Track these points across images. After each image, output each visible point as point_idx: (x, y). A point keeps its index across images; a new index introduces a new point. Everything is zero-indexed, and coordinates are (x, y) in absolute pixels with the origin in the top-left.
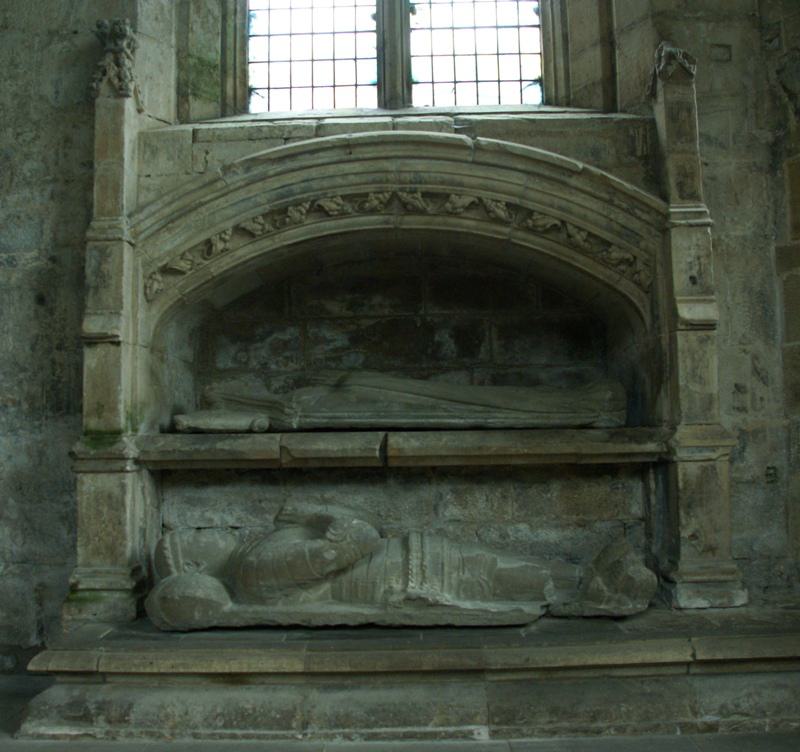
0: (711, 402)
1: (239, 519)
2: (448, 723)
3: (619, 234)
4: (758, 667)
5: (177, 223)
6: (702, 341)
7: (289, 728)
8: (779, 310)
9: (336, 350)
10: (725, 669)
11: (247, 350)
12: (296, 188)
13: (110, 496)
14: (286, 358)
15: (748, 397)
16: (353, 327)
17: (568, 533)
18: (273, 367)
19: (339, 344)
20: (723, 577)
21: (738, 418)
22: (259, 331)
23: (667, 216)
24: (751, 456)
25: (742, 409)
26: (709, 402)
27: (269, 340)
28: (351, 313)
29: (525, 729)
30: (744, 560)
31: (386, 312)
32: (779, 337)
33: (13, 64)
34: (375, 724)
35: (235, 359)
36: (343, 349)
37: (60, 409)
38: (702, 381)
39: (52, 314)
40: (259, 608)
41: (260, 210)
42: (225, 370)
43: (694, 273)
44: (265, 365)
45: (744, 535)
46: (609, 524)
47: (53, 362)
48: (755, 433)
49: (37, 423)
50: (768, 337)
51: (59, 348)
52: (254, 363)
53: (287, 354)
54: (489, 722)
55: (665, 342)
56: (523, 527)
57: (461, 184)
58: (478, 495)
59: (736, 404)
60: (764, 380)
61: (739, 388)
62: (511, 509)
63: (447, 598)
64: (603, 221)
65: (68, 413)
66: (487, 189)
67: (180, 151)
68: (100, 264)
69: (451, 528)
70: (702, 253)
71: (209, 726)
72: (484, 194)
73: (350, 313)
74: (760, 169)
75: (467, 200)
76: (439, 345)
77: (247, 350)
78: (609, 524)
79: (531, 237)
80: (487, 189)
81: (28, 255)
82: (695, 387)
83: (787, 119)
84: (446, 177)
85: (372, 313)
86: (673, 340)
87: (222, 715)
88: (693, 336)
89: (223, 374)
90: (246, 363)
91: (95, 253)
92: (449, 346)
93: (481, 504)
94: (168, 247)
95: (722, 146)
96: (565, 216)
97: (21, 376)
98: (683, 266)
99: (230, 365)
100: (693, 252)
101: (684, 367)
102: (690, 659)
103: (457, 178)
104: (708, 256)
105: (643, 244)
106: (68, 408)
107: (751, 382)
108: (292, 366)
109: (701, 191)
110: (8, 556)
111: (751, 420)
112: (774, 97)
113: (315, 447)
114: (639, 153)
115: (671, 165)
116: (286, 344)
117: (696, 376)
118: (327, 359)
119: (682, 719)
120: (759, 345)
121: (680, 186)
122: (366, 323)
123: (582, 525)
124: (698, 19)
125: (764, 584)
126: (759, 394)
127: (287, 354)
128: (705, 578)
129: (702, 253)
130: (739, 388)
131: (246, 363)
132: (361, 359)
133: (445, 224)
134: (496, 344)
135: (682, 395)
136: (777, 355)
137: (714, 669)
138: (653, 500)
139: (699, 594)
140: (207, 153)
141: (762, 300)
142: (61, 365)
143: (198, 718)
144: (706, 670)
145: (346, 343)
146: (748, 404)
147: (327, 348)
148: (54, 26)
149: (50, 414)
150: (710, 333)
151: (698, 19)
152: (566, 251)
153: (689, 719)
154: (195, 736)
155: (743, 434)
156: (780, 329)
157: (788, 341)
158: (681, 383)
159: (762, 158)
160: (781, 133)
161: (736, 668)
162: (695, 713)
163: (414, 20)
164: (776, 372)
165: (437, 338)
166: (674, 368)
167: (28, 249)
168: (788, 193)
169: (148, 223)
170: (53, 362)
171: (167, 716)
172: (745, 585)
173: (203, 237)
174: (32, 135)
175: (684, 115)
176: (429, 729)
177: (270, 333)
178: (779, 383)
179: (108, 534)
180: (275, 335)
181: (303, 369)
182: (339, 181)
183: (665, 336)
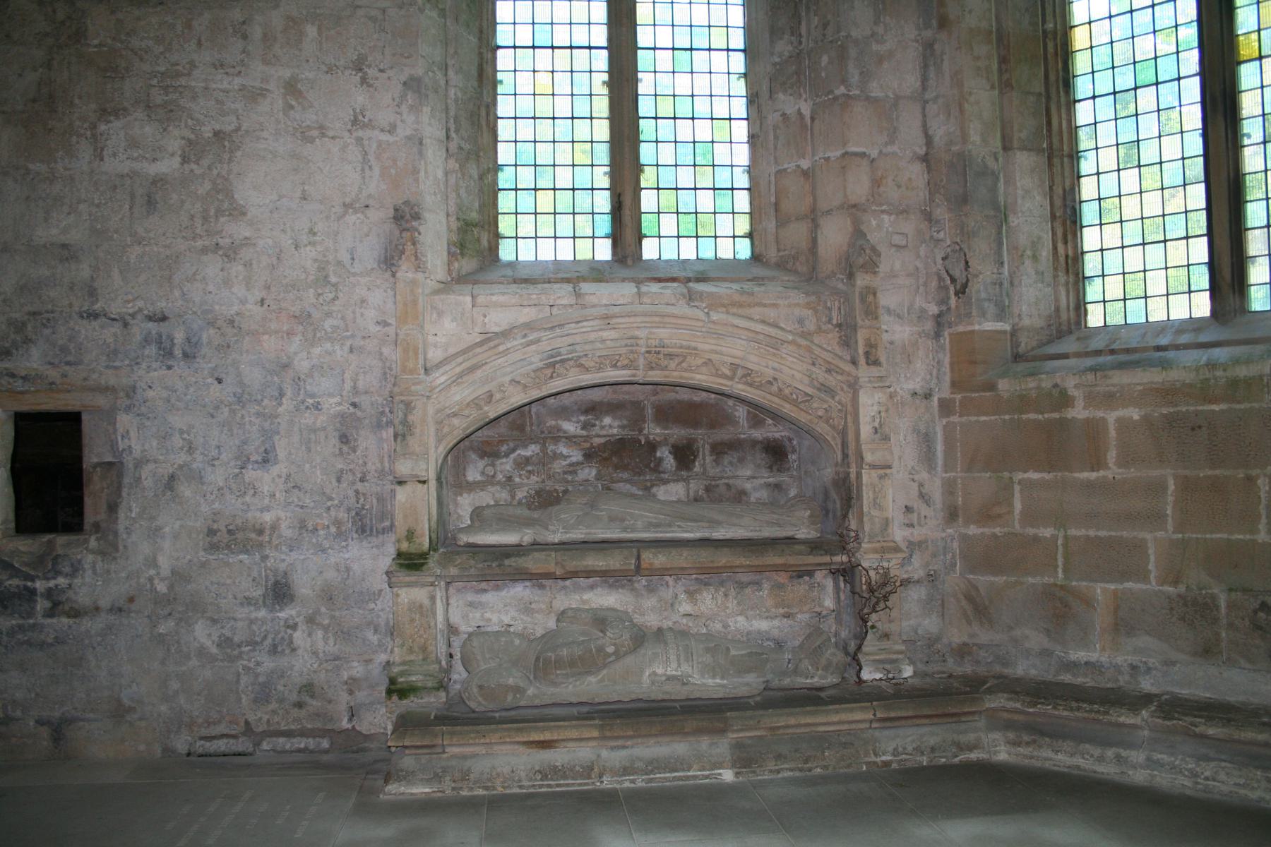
0: (887, 525)
1: (513, 618)
2: (703, 769)
3: (819, 389)
4: (918, 721)
5: (465, 378)
6: (881, 477)
7: (589, 777)
8: (940, 448)
9: (571, 465)
10: (897, 723)
11: (493, 465)
12: (563, 351)
13: (421, 606)
14: (529, 472)
15: (915, 515)
16: (587, 445)
17: (776, 623)
18: (517, 480)
19: (574, 459)
20: (895, 657)
21: (907, 532)
22: (504, 448)
23: (857, 378)
24: (917, 561)
25: (911, 525)
26: (886, 523)
27: (512, 456)
28: (584, 433)
29: (758, 771)
30: (909, 642)
31: (615, 431)
32: (939, 469)
33: (312, 232)
34: (652, 772)
35: (483, 473)
36: (578, 463)
37: (363, 531)
38: (881, 508)
39: (355, 451)
40: (552, 690)
41: (533, 367)
42: (475, 483)
43: (876, 424)
44: (510, 479)
45: (912, 622)
46: (807, 616)
47: (357, 492)
48: (920, 543)
49: (344, 544)
50: (931, 467)
51: (362, 480)
52: (500, 477)
53: (530, 468)
54: (733, 766)
55: (853, 476)
56: (740, 618)
57: (695, 349)
58: (705, 594)
59: (907, 521)
60: (928, 503)
61: (908, 509)
62: (732, 604)
63: (697, 679)
64: (806, 380)
65: (371, 535)
66: (717, 353)
67: (463, 314)
68: (406, 415)
69: (684, 621)
70: (882, 409)
71: (531, 780)
72: (714, 357)
73: (584, 433)
74: (927, 336)
75: (700, 362)
76: (661, 460)
77: (493, 465)
78: (807, 616)
79: (749, 389)
80: (717, 353)
81: (332, 400)
82: (875, 513)
83: (949, 298)
84: (684, 343)
85: (604, 432)
86: (859, 475)
87: (540, 772)
88: (874, 473)
89: (472, 487)
90: (493, 476)
91: (401, 406)
92: (669, 461)
93: (708, 601)
94: (457, 398)
95: (899, 316)
96: (778, 375)
97: (329, 503)
98: (868, 419)
99: (479, 478)
100: (875, 408)
101: (867, 496)
102: (585, 287)
103: (693, 344)
104: (887, 411)
105: (837, 398)
106: (371, 530)
107: (917, 504)
108: (534, 478)
109: (883, 359)
110: (321, 655)
111: (917, 534)
112: (940, 279)
113: (585, 563)
114: (835, 322)
115: (861, 336)
116: (527, 460)
117: (876, 504)
118: (565, 473)
119: (867, 759)
120: (924, 475)
121: (867, 354)
122: (597, 441)
123: (787, 616)
124: (883, 212)
125: (925, 659)
126: (923, 514)
127: (530, 468)
128: (882, 657)
129: (882, 409)
130: (908, 509)
131: (493, 476)
132: (594, 472)
133: (681, 377)
134: (709, 459)
135: (865, 519)
136: (938, 482)
137: (888, 724)
138: (842, 597)
139: (877, 670)
140: (485, 316)
141: (926, 440)
142: (364, 494)
143: (523, 774)
144: (882, 725)
145: (580, 458)
146: (915, 523)
147: (564, 463)
148: (348, 200)
149: (355, 536)
150: (888, 471)
151: (883, 212)
152: (776, 400)
153: (873, 758)
154: (520, 787)
155: (911, 544)
156: (940, 462)
157: (946, 472)
158: (865, 509)
159: (929, 326)
160: (944, 308)
161: (903, 722)
162: (876, 755)
163: (605, 77)
164: (937, 496)
165: (658, 454)
166: (860, 497)
167: (331, 395)
168: (948, 355)
169: (443, 379)
170: (357, 492)
171: (498, 775)
172: (912, 662)
173: (486, 388)
174: (331, 296)
175: (871, 298)
176: (691, 773)
177: (514, 450)
178: (939, 506)
179: (421, 636)
180: (518, 452)
181: (543, 481)
182: (599, 345)
183: (853, 471)
